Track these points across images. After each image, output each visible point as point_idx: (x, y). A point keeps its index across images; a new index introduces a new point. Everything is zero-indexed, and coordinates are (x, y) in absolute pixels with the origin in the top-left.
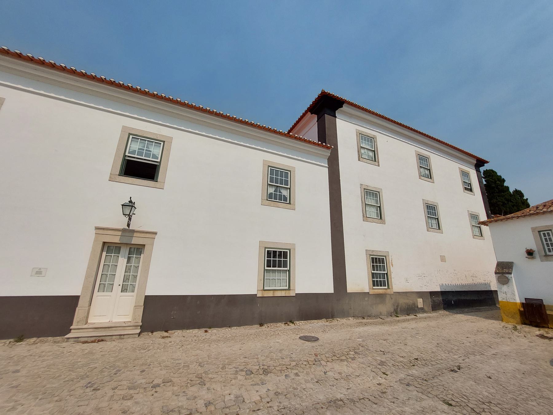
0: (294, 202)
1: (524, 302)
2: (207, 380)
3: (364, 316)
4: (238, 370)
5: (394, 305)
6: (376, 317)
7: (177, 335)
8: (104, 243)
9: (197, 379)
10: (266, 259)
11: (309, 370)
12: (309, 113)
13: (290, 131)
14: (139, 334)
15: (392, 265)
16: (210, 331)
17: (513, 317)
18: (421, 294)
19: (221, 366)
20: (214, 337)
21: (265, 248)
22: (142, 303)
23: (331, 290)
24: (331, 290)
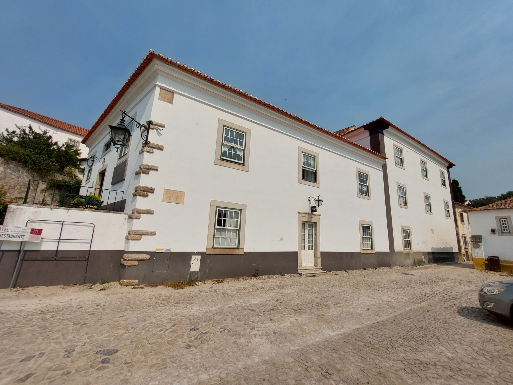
10: (217, 218)
17: (481, 266)
18: (424, 253)
21: (217, 207)
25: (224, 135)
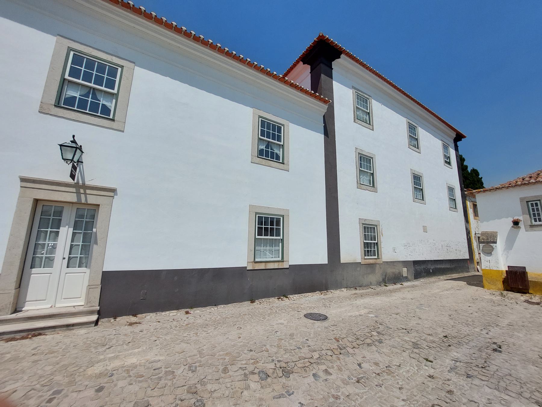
0: (288, 162)
1: (507, 269)
2: (206, 395)
3: (356, 285)
4: (246, 371)
5: (383, 275)
6: (368, 286)
7: (150, 319)
8: (36, 201)
9: (190, 396)
10: (257, 226)
11: (339, 363)
12: (301, 63)
13: (286, 75)
14: (96, 323)
15: (382, 234)
16: (191, 311)
18: (405, 263)
19: (221, 368)
20: (199, 321)
21: (256, 213)
22: (99, 282)
23: (325, 261)
24: (325, 261)
25: (260, 128)
